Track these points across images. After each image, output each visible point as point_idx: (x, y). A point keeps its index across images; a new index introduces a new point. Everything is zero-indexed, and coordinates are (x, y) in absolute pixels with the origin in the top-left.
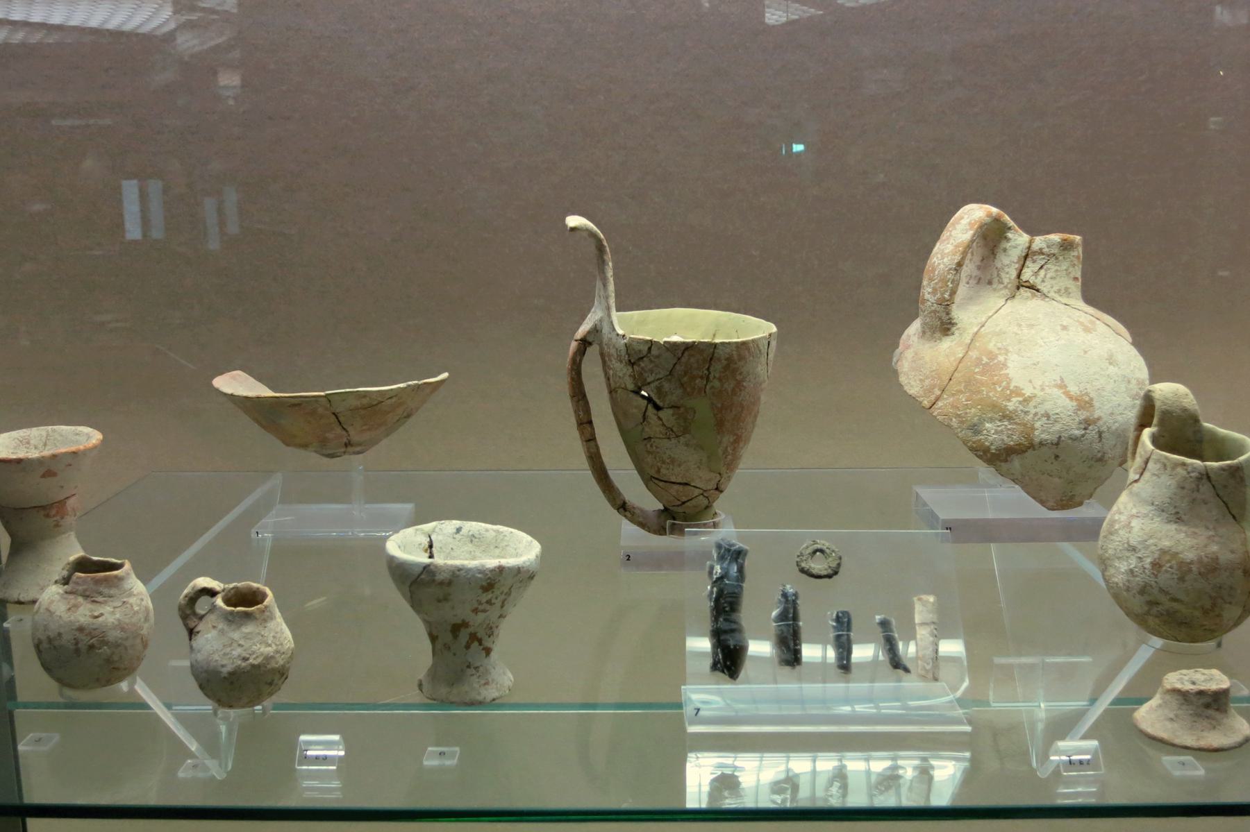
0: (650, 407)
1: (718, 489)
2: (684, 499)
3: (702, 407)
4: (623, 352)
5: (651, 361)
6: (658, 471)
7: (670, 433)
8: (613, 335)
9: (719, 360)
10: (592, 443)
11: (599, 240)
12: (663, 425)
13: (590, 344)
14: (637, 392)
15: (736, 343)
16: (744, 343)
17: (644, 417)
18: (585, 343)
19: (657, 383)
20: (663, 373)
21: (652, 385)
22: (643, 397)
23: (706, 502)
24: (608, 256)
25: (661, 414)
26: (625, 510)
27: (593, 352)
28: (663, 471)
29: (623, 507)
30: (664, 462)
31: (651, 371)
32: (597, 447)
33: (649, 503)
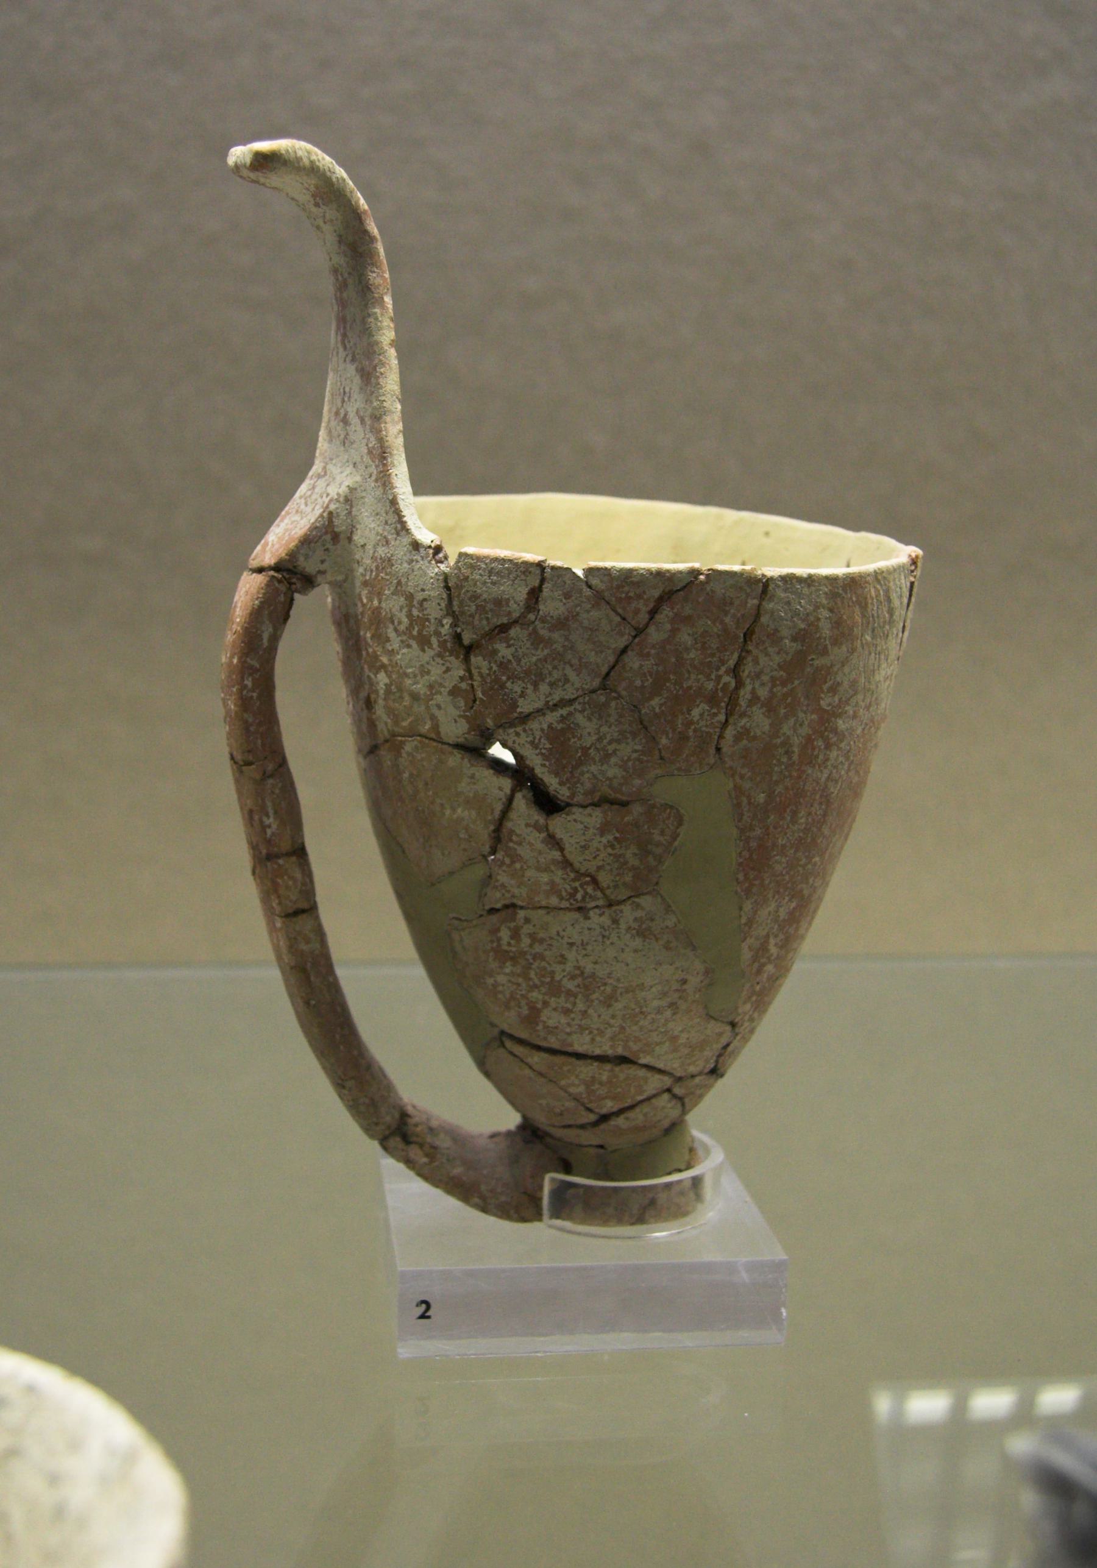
0: (522, 803)
1: (715, 1072)
2: (609, 1106)
3: (700, 797)
4: (434, 611)
5: (537, 640)
6: (532, 1017)
7: (585, 892)
8: (399, 549)
9: (774, 637)
10: (304, 924)
11: (356, 216)
12: (566, 864)
13: (309, 582)
14: (476, 751)
15: (832, 580)
16: (853, 583)
17: (499, 836)
18: (290, 577)
19: (552, 718)
20: (578, 682)
21: (534, 725)
22: (498, 765)
23: (674, 1113)
24: (381, 276)
25: (558, 824)
26: (406, 1139)
27: (313, 610)
28: (551, 1018)
29: (400, 1132)
30: (555, 989)
31: (536, 677)
32: (320, 933)
33: (481, 1111)
